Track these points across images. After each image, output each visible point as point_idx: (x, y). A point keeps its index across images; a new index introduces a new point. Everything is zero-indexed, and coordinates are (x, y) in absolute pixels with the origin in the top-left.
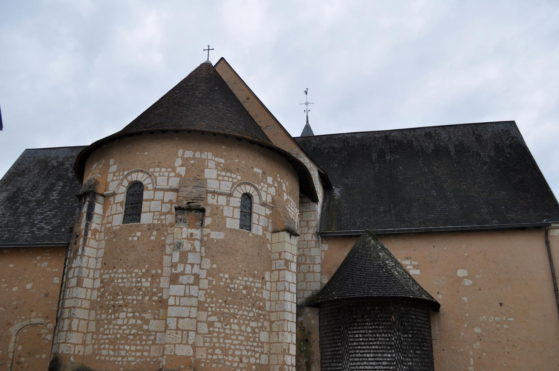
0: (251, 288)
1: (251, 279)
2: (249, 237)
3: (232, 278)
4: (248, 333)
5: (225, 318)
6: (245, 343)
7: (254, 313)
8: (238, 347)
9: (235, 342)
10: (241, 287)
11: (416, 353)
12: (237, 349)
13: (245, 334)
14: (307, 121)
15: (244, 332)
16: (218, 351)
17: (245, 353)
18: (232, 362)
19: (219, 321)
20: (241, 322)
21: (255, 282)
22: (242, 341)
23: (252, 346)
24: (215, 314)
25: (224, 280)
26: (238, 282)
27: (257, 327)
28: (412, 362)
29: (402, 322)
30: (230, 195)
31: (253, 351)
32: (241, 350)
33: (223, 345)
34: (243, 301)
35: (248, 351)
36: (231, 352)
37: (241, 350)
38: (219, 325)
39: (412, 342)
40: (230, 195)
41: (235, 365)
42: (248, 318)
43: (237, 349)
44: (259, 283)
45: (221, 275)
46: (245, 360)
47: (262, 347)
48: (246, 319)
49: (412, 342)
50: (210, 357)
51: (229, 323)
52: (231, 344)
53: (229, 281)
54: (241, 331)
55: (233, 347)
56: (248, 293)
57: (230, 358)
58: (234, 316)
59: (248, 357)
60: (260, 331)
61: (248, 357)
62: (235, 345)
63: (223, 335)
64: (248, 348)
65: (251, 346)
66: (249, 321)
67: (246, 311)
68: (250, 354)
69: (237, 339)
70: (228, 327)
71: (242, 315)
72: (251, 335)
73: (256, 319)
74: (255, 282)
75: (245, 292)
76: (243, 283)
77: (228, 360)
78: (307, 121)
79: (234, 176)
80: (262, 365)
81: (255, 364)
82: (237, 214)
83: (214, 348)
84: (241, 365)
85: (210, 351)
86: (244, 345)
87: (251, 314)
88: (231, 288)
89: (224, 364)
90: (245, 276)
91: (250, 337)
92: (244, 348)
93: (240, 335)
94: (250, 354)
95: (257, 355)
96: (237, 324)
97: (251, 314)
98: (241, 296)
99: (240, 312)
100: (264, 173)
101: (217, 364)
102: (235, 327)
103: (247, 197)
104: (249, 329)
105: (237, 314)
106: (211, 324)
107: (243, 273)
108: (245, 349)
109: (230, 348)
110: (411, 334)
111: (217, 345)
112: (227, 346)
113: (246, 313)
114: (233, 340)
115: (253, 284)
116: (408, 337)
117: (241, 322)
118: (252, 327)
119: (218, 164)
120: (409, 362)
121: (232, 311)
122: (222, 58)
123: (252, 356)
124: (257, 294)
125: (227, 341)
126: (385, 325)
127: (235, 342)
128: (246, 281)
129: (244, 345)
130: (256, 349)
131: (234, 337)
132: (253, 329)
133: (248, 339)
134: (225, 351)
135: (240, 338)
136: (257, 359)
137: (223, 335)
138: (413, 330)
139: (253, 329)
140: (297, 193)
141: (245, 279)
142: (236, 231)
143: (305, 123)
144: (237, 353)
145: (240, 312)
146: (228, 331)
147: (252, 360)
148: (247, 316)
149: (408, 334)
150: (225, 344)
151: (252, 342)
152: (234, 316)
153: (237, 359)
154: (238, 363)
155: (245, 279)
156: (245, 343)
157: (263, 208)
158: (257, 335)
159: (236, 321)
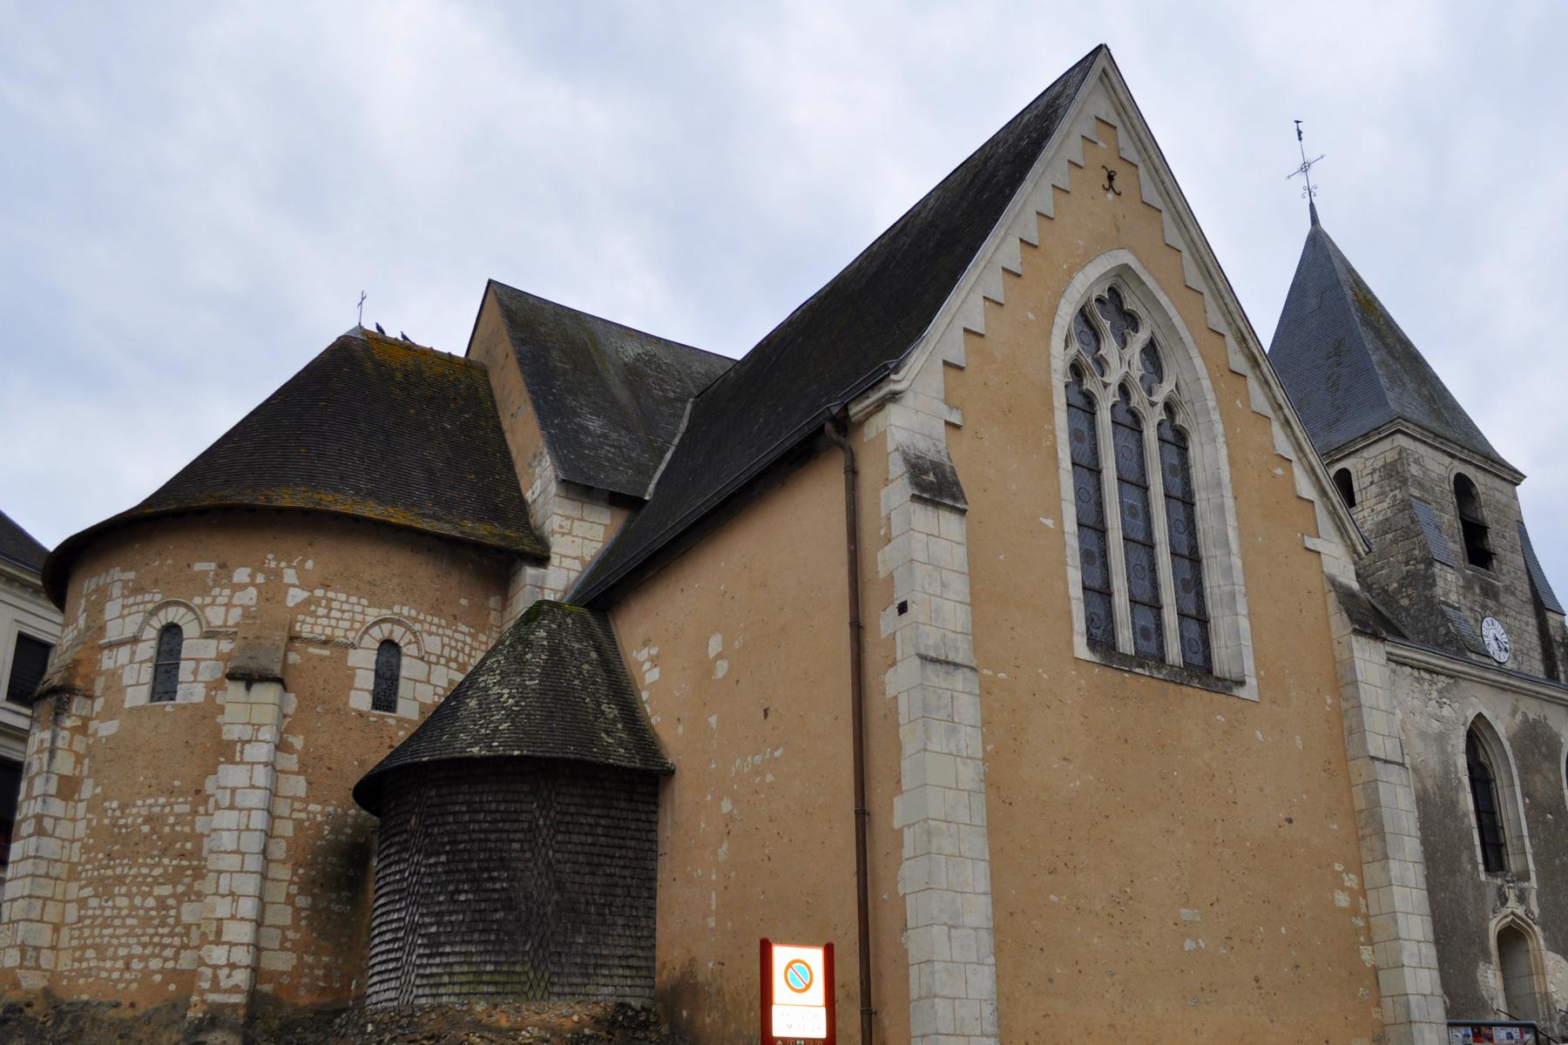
0: (162, 818)
1: (162, 800)
2: (165, 714)
3: (123, 807)
4: (148, 910)
5: (104, 887)
6: (139, 931)
7: (166, 868)
8: (123, 940)
9: (120, 932)
10: (140, 820)
11: (455, 902)
12: (121, 945)
13: (141, 912)
14: (1314, 220)
15: (137, 908)
16: (90, 953)
17: (138, 950)
18: (110, 971)
19: (96, 895)
20: (134, 889)
21: (171, 805)
22: (132, 927)
23: (156, 934)
24: (90, 882)
25: (110, 813)
26: (135, 811)
27: (174, 896)
28: (438, 924)
29: (427, 827)
30: (135, 640)
31: (155, 945)
32: (129, 946)
33: (98, 940)
34: (140, 848)
35: (144, 946)
36: (110, 952)
37: (129, 946)
38: (94, 902)
39: (446, 873)
40: (135, 640)
41: (116, 975)
42: (150, 880)
43: (121, 945)
44: (185, 803)
45: (107, 804)
46: (136, 965)
47: (187, 934)
48: (143, 883)
49: (446, 873)
50: (76, 965)
51: (112, 897)
52: (112, 936)
53: (118, 813)
54: (133, 907)
55: (115, 941)
56: (153, 830)
57: (108, 964)
58: (120, 880)
59: (143, 958)
60: (180, 903)
61: (143, 958)
62: (118, 937)
63: (99, 921)
64: (146, 939)
65: (151, 937)
66: (151, 885)
67: (146, 865)
68: (148, 951)
69: (123, 926)
70: (110, 904)
71: (135, 877)
72: (153, 913)
73: (173, 878)
74: (171, 805)
75: (146, 829)
76: (144, 811)
77: (104, 969)
78: (1314, 220)
79: (148, 597)
80: (183, 972)
81: (161, 971)
82: (147, 673)
83: (84, 948)
84: (127, 975)
85: (77, 954)
86: (137, 936)
87: (157, 872)
88: (120, 827)
89: (97, 977)
90: (150, 795)
91: (153, 918)
92: (135, 940)
93: (129, 916)
94: (148, 951)
95: (168, 952)
96: (126, 895)
97: (157, 872)
98: (137, 839)
99: (134, 871)
100: (222, 566)
101: (87, 977)
102: (122, 902)
103: (171, 632)
104: (151, 902)
105: (126, 876)
106: (82, 903)
107: (145, 791)
108: (139, 943)
109: (109, 945)
110: (447, 853)
111: (89, 942)
112: (106, 940)
113: (145, 871)
114: (116, 927)
115: (167, 810)
116: (436, 864)
117: (134, 889)
118: (158, 898)
119: (125, 584)
120: (431, 924)
121: (119, 871)
122: (490, 282)
123: (153, 956)
124: (178, 828)
125: (105, 932)
126: (398, 843)
127: (120, 932)
128: (151, 806)
129: (137, 936)
130: (166, 941)
131: (117, 922)
132: (161, 901)
133: (146, 922)
134: (100, 950)
135: (129, 922)
136: (166, 960)
137: (99, 921)
138: (454, 842)
139: (161, 901)
140: (53, 606)
141: (149, 801)
142: (143, 708)
143: (1307, 227)
144: (122, 952)
145: (134, 871)
146: (108, 913)
147: (155, 964)
148: (145, 876)
149: (438, 854)
150: (101, 936)
151: (156, 927)
152: (120, 880)
153: (120, 964)
154: (122, 972)
155: (149, 801)
156: (139, 931)
157: (213, 643)
158: (172, 912)
159: (124, 890)
